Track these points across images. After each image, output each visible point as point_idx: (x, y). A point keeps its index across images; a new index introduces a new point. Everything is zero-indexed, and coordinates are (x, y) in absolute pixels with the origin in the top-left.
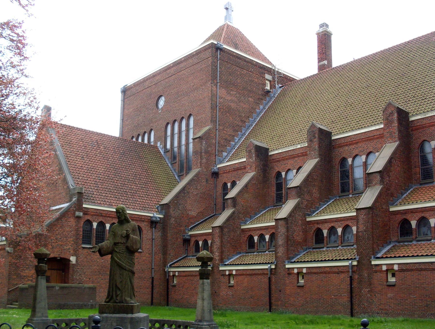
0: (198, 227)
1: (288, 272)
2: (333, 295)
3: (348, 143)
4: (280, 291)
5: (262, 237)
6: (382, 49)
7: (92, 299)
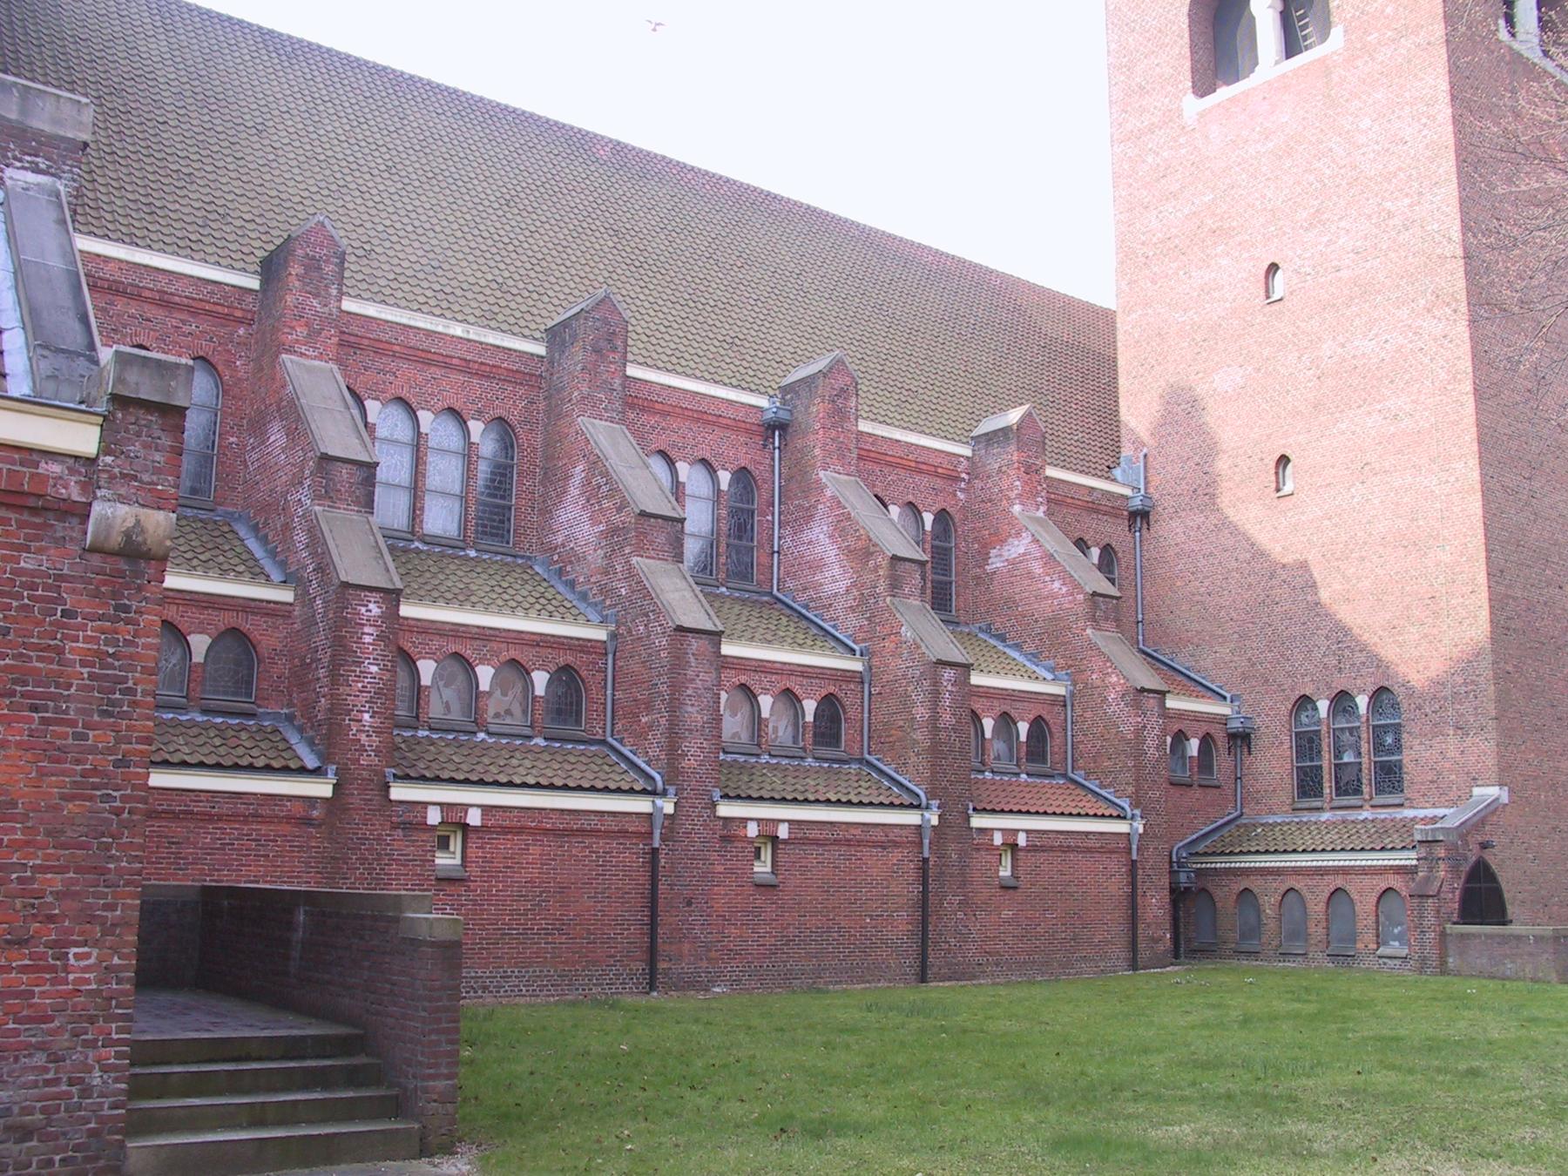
3: (640, 402)
4: (689, 904)
6: (889, 230)
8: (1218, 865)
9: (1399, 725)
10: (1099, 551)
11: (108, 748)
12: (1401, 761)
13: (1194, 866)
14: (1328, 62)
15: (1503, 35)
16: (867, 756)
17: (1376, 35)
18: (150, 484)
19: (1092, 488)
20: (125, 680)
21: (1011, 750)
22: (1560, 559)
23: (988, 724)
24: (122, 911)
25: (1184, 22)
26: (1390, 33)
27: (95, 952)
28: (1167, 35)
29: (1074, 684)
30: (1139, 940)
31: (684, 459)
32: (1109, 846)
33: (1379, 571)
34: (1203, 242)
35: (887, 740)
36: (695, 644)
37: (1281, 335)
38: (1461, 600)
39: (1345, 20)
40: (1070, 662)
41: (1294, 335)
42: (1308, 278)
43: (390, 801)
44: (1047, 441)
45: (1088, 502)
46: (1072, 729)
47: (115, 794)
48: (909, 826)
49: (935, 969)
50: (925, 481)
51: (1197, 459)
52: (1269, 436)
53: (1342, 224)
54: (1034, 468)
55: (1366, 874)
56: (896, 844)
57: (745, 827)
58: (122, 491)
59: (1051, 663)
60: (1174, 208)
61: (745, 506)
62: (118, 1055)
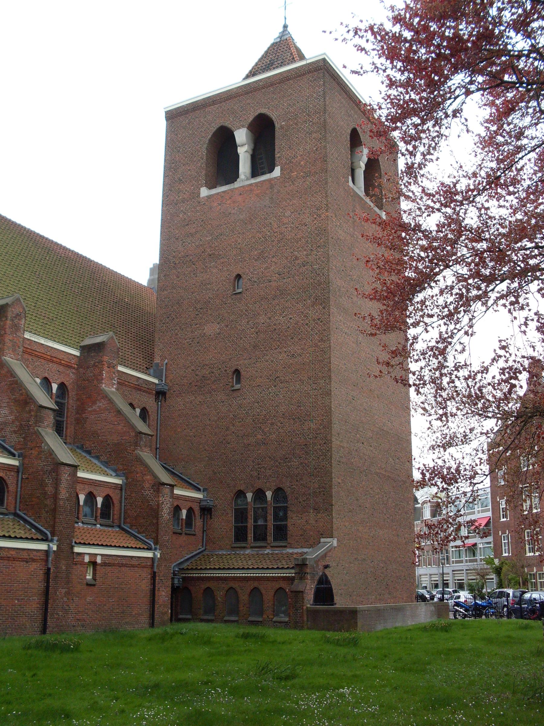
0: (183, 484)
2: (17, 599)
8: (194, 575)
9: (287, 507)
10: (140, 410)
12: (286, 524)
13: (182, 575)
14: (272, 182)
16: (18, 512)
19: (139, 378)
21: (92, 511)
22: (363, 430)
23: (82, 497)
25: (204, 151)
28: (195, 156)
29: (127, 479)
30: (156, 612)
33: (280, 430)
34: (204, 260)
38: (319, 447)
39: (282, 164)
43: (74, 553)
44: (120, 353)
49: (51, 629)
51: (193, 367)
52: (230, 359)
53: (274, 260)
59: (115, 467)
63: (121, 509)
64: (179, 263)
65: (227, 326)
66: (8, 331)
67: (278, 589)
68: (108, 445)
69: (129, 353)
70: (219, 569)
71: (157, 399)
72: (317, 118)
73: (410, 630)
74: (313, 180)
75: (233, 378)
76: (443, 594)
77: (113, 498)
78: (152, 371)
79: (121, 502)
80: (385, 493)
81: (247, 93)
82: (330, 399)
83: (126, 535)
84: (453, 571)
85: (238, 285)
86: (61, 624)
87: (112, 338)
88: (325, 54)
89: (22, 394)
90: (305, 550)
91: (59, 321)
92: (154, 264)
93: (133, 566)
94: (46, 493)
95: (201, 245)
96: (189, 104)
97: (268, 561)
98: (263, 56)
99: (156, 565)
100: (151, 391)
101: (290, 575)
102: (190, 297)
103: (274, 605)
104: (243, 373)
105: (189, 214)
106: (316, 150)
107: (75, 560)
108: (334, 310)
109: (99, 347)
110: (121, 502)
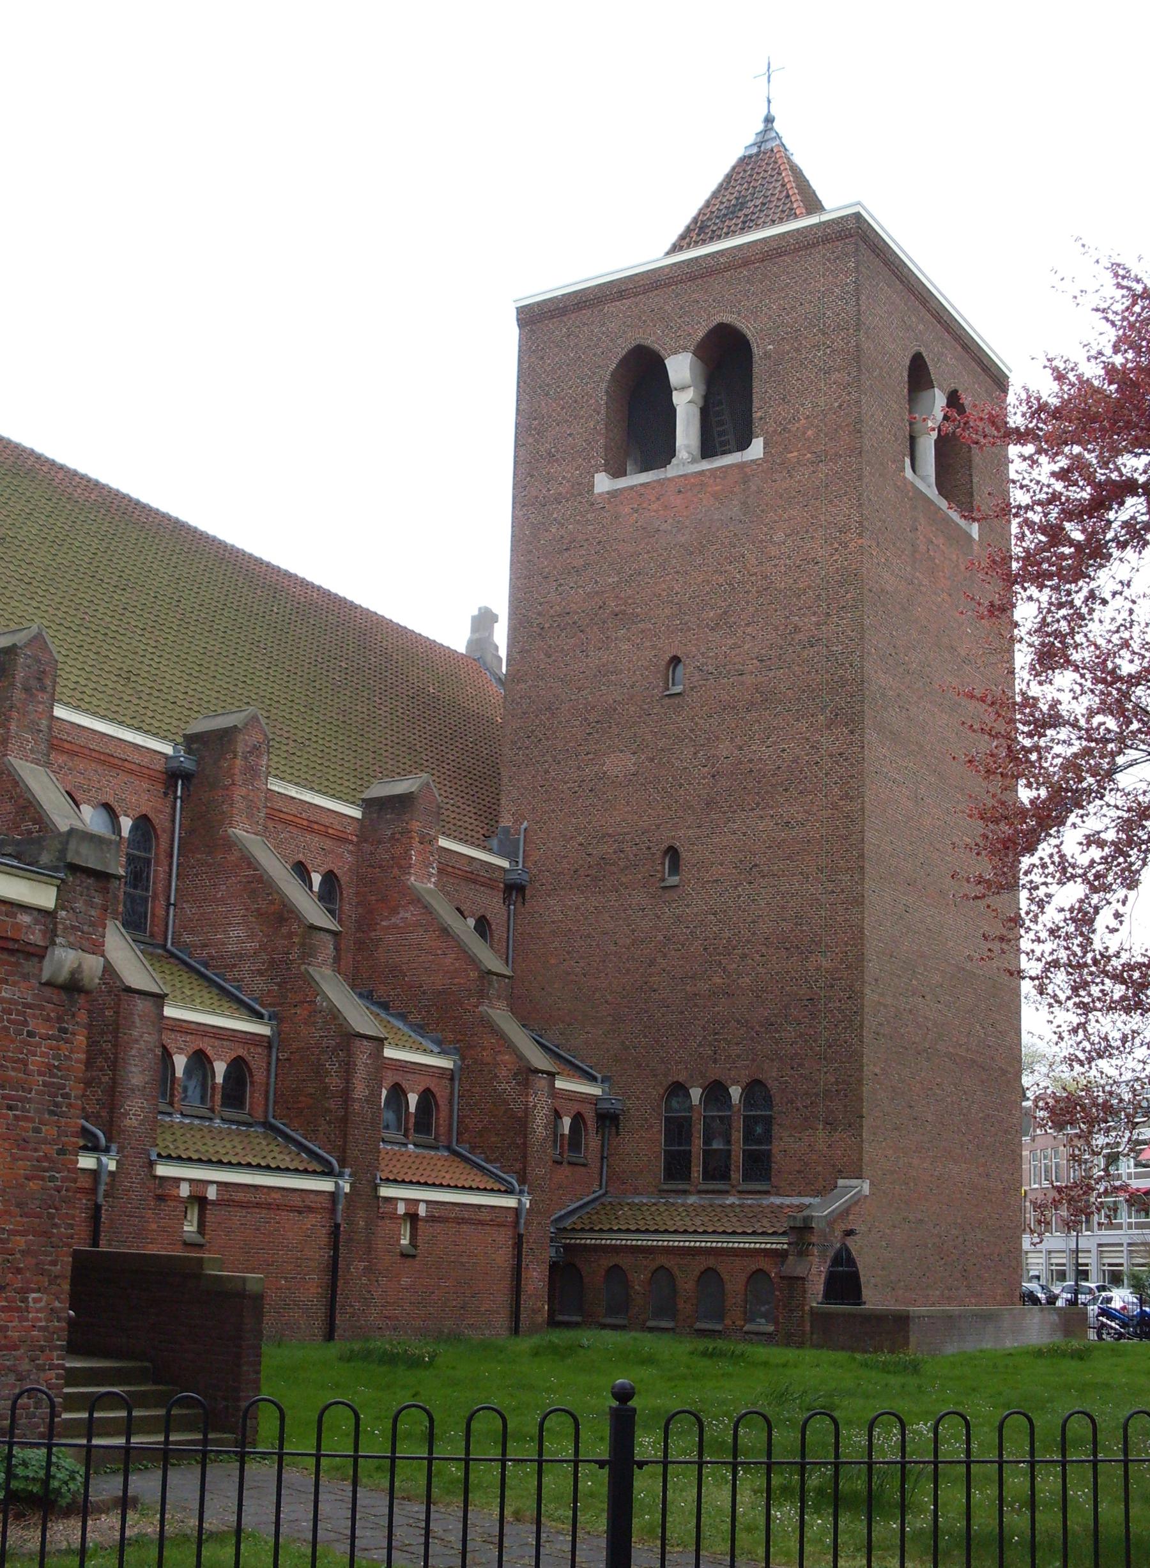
0: (185, 976)
1: (159, 1192)
5: (200, 1061)
7: (424, 1359)
8: (588, 1241)
11: (53, 1140)
12: (770, 1150)
13: (563, 1241)
15: (908, 472)
16: (273, 1121)
17: (796, 454)
18: (88, 934)
20: (63, 1087)
21: (399, 1119)
24: (61, 1266)
25: (601, 397)
26: (809, 455)
27: (45, 1297)
28: (583, 407)
29: (463, 1059)
31: (88, 802)
32: (498, 1220)
33: (760, 969)
34: (604, 622)
35: (295, 1106)
36: (141, 1005)
37: (678, 728)
40: (459, 1037)
41: (692, 730)
42: (710, 677)
43: (378, 1197)
45: (467, 872)
46: (459, 1103)
47: (57, 1175)
48: (324, 1192)
50: (315, 841)
51: (580, 839)
52: (658, 826)
53: (749, 630)
54: (428, 838)
55: (737, 1256)
56: (310, 1210)
57: (178, 1187)
58: (72, 939)
60: (576, 583)
61: (143, 854)
62: (58, 1377)
63: (451, 1117)
64: (551, 627)
65: (652, 760)
66: (239, 779)
67: (754, 1272)
68: (424, 993)
69: (448, 806)
70: (638, 1231)
71: (507, 900)
72: (842, 339)
73: (1010, 1354)
74: (832, 470)
75: (663, 864)
76: (1076, 1293)
77: (438, 1095)
78: (495, 843)
79: (451, 1102)
80: (965, 1093)
81: (693, 279)
82: (862, 912)
83: (463, 1165)
84: (1100, 1245)
85: (673, 679)
86: (358, 1324)
87: (428, 784)
88: (859, 203)
89: (272, 902)
90: (807, 1200)
91: (315, 746)
92: (480, 609)
93: (481, 1223)
94: (326, 1089)
95: (597, 593)
96: (569, 294)
97: (734, 1220)
98: (721, 185)
99: (522, 1221)
100: (496, 884)
101: (779, 1246)
102: (573, 697)
103: (746, 1302)
104: (684, 855)
105: (570, 527)
106: (840, 406)
107: (381, 1210)
108: (871, 736)
109: (403, 803)
110: (451, 1102)
